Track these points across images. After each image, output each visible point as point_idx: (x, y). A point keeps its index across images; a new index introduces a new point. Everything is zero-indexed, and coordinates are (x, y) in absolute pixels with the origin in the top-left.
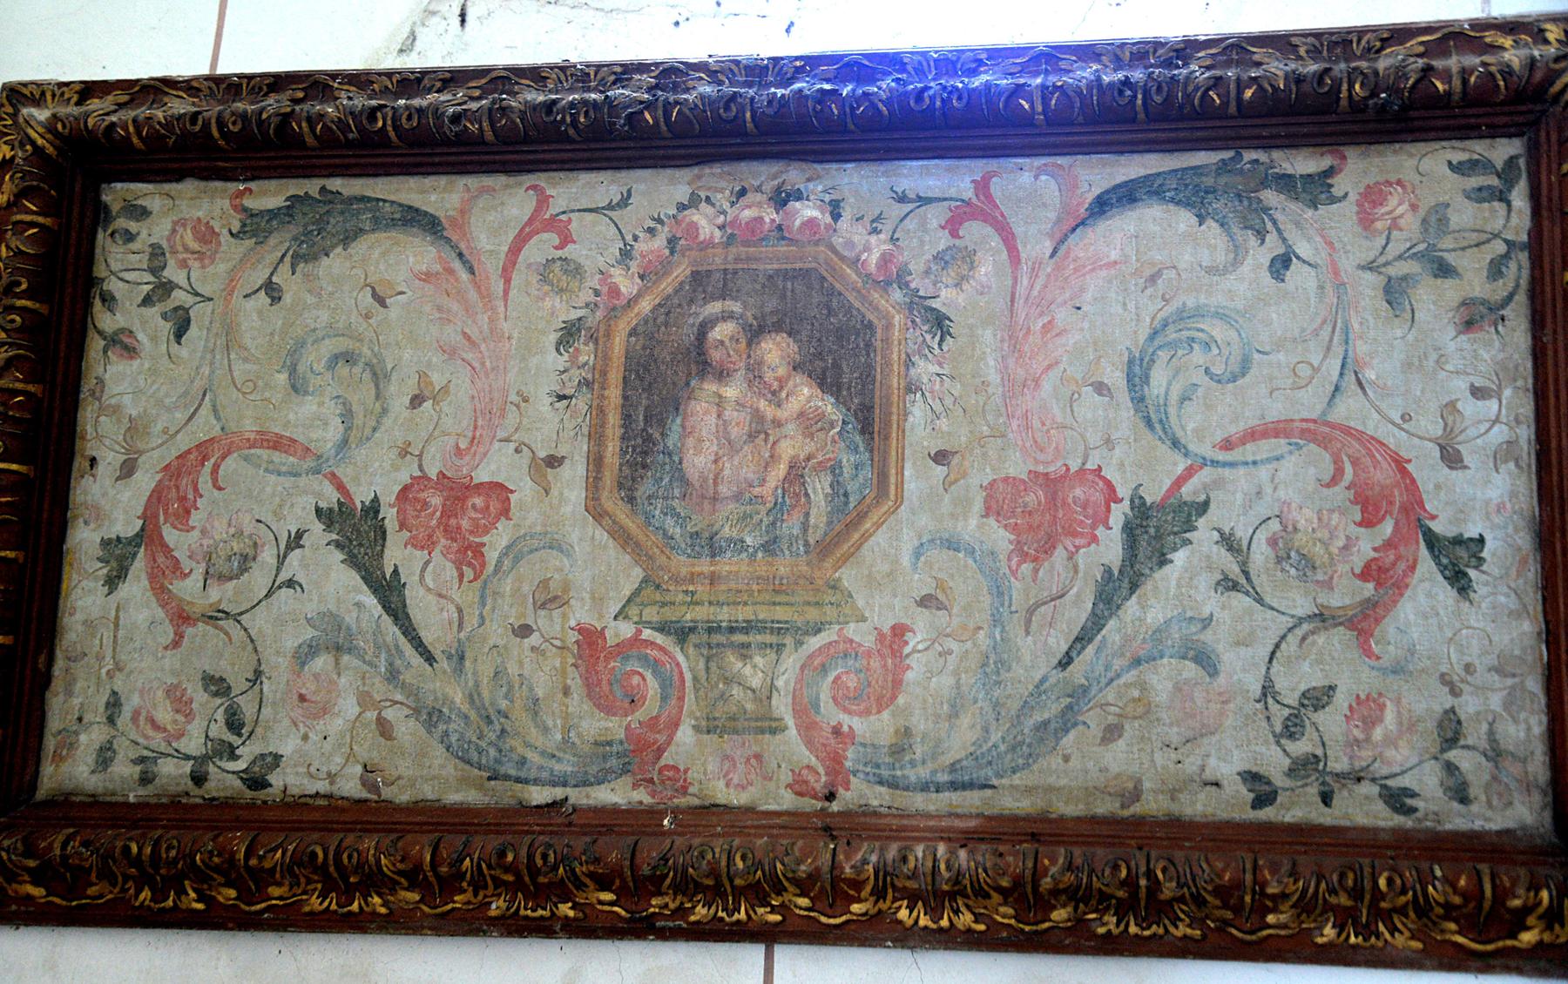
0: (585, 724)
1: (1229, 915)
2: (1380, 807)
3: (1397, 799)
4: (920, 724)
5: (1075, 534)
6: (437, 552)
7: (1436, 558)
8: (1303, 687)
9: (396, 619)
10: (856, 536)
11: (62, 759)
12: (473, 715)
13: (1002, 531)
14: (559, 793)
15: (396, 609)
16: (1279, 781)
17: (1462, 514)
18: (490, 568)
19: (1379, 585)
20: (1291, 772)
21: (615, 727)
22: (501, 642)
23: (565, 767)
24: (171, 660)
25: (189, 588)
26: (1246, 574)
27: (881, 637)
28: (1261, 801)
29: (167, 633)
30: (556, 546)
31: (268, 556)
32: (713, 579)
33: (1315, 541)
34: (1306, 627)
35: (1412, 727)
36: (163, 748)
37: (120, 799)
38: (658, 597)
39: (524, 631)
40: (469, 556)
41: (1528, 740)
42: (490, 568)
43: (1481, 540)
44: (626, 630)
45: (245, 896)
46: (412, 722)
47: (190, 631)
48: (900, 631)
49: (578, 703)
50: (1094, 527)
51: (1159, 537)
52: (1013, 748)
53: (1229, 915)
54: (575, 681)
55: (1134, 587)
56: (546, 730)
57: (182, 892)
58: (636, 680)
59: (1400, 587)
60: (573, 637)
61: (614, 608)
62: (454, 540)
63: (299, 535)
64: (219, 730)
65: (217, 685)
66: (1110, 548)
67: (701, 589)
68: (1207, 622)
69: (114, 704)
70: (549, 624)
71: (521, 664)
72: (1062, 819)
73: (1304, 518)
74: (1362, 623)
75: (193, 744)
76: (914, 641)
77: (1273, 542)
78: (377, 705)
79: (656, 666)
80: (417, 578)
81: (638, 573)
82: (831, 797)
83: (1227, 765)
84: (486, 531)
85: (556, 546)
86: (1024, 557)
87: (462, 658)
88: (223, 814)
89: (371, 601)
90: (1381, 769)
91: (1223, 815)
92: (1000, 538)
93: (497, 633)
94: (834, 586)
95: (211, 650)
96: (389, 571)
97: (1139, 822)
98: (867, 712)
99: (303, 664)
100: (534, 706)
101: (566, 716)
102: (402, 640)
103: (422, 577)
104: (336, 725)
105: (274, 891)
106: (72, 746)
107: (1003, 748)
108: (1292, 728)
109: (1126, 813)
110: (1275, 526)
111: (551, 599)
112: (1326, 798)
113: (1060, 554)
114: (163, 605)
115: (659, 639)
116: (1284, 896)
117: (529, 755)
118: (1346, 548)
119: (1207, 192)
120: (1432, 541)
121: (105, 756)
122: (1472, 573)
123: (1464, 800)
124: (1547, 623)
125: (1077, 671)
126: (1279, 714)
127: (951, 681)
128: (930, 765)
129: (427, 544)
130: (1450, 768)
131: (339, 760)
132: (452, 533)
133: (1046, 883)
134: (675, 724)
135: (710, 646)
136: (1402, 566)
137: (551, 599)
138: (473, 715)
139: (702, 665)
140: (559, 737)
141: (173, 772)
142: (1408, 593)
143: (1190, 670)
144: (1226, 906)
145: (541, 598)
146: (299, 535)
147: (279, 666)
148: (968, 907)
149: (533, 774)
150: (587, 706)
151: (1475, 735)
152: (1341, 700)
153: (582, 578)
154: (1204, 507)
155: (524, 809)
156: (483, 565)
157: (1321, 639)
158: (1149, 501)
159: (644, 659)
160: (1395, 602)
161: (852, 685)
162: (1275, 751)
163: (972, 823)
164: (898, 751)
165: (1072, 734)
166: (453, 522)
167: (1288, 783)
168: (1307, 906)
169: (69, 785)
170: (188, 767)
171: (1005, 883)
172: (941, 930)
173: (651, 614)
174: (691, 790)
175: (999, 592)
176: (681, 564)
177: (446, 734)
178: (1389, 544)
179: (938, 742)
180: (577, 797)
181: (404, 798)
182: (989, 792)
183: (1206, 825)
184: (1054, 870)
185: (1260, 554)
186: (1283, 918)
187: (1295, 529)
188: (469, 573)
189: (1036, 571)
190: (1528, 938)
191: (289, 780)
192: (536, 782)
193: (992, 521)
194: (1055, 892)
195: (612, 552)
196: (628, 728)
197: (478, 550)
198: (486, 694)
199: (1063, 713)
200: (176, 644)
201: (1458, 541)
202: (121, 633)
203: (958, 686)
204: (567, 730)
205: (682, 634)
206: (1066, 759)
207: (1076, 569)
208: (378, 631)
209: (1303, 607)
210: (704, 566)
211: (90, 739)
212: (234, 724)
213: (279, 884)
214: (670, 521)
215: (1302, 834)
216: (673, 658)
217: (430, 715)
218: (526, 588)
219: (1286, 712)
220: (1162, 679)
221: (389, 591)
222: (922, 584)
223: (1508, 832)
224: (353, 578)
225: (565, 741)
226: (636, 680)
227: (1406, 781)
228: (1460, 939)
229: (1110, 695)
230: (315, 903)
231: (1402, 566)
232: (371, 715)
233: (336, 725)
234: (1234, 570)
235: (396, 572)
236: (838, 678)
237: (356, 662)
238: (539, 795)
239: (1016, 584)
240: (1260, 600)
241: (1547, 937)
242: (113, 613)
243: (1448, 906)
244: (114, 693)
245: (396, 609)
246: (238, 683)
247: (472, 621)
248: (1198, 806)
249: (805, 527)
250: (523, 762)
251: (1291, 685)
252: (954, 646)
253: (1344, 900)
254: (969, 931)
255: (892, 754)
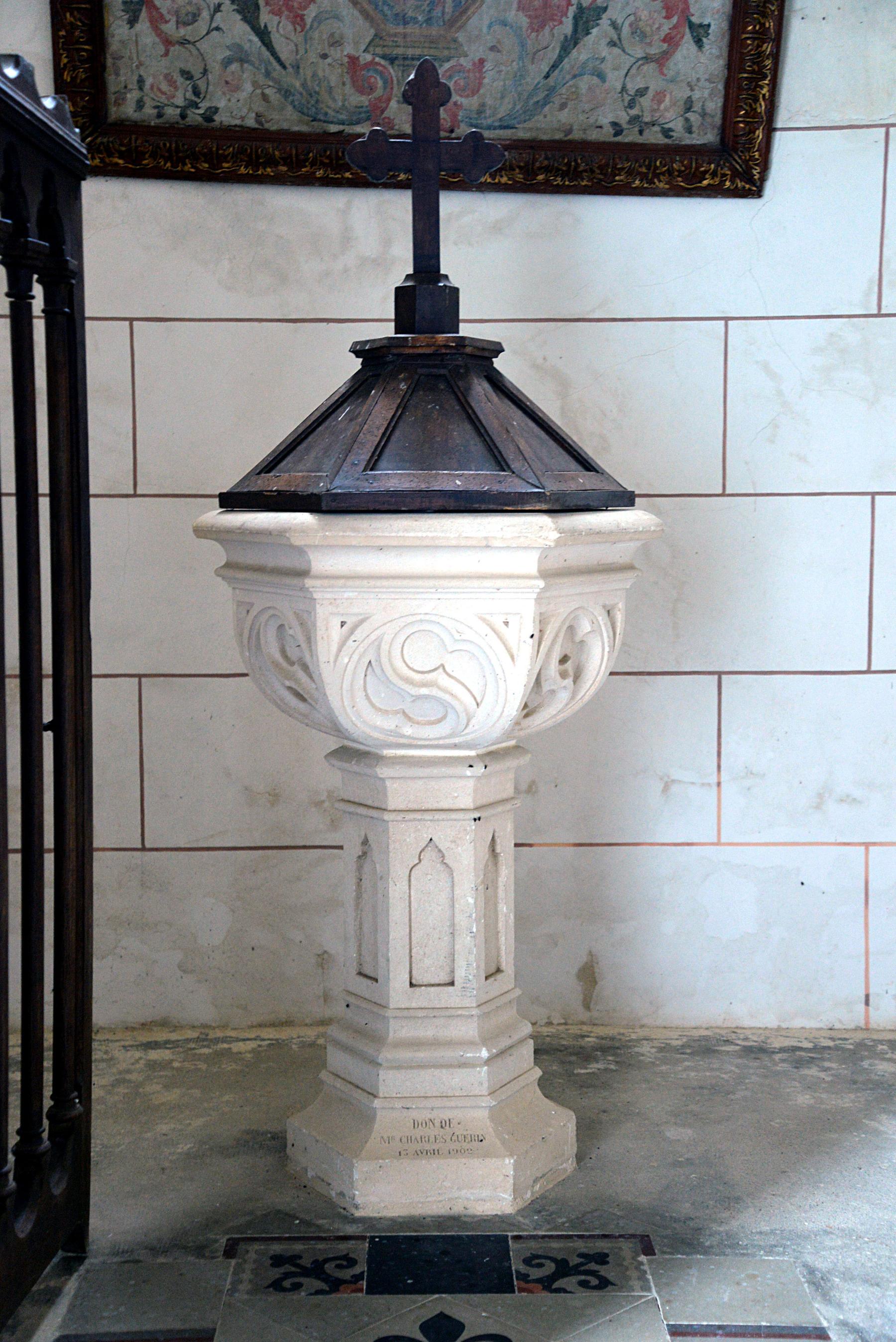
0: (351, 99)
1: (602, 177)
2: (660, 136)
3: (667, 133)
4: (489, 101)
5: (554, 20)
6: (283, 18)
7: (692, 33)
8: (637, 87)
9: (268, 49)
10: (464, 18)
11: (119, 105)
12: (304, 93)
13: (524, 18)
14: (341, 127)
15: (267, 44)
16: (625, 126)
17: (703, 14)
18: (308, 27)
19: (669, 45)
20: (629, 122)
21: (364, 100)
22: (314, 60)
23: (343, 117)
24: (164, 62)
25: (169, 28)
26: (620, 39)
27: (474, 64)
28: (616, 135)
29: (161, 49)
30: (337, 17)
31: (205, 14)
32: (405, 36)
33: (647, 25)
34: (640, 62)
35: (674, 104)
36: (166, 102)
37: (146, 124)
38: (381, 42)
39: (324, 56)
40: (298, 20)
41: (716, 109)
42: (308, 27)
43: (709, 25)
44: (368, 57)
45: (213, 166)
46: (278, 95)
47: (172, 48)
48: (482, 61)
49: (348, 89)
50: (562, 16)
51: (587, 22)
52: (525, 112)
53: (602, 177)
54: (347, 79)
55: (576, 44)
56: (334, 100)
57: (184, 164)
58: (373, 80)
59: (677, 45)
60: (346, 60)
61: (363, 47)
62: (290, 12)
63: (220, 5)
64: (190, 95)
65: (187, 75)
66: (567, 27)
67: (400, 40)
68: (603, 60)
69: (141, 81)
70: (335, 53)
71: (324, 71)
72: (541, 141)
73: (644, 15)
74: (661, 60)
75: (180, 101)
76: (488, 66)
77: (631, 25)
78: (260, 87)
79: (381, 74)
80: (275, 29)
81: (372, 31)
82: (452, 131)
83: (605, 120)
84: (305, 8)
85: (337, 17)
86: (533, 30)
87: (298, 67)
88: (195, 132)
89: (255, 39)
90: (662, 121)
91: (602, 139)
92: (524, 21)
93: (313, 57)
94: (455, 40)
95: (182, 58)
96: (262, 25)
97: (570, 142)
98: (467, 96)
99: (226, 67)
100: (330, 90)
101: (344, 95)
102: (272, 59)
103: (278, 29)
104: (243, 95)
105: (225, 165)
106: (124, 99)
107: (521, 112)
108: (631, 105)
109: (566, 139)
110: (632, 18)
111: (336, 42)
112: (641, 132)
113: (547, 29)
114: (158, 35)
115: (383, 62)
116: (623, 169)
117: (330, 111)
118: (659, 28)
119: (842, 1249)
120: (691, 26)
121: (140, 104)
122: (704, 40)
123: (690, 132)
124: (729, 60)
125: (551, 81)
126: (627, 98)
127: (502, 83)
128: (492, 119)
129: (278, 13)
130: (687, 120)
131: (246, 111)
132: (290, 9)
133: (537, 164)
134: (389, 100)
135: (404, 66)
136: (679, 36)
137: (336, 42)
138: (304, 93)
139: (400, 74)
140: (340, 104)
141: (171, 113)
142: (680, 48)
143: (595, 80)
144: (601, 174)
145: (331, 41)
146: (220, 5)
147: (215, 68)
148: (507, 175)
149: (331, 119)
150: (352, 91)
151: (697, 107)
152: (651, 93)
153: (349, 33)
154: (605, 9)
155: (327, 134)
156: (305, 24)
157: (645, 68)
158: (584, 5)
159: (376, 71)
160: (674, 52)
161: (462, 84)
162: (624, 113)
163: (508, 142)
164: (479, 112)
165: (547, 107)
166: (290, 3)
167: (628, 126)
168: (630, 172)
169: (123, 116)
170: (178, 111)
171: (522, 164)
172: (495, 184)
173: (379, 50)
174: (397, 127)
175: (523, 45)
176: (392, 28)
177: (293, 101)
178: (675, 27)
179: (495, 109)
180: (349, 129)
181: (274, 128)
182: (514, 130)
183: (595, 143)
184: (541, 160)
185: (626, 31)
186: (622, 177)
187: (640, 20)
188: (299, 29)
189: (537, 36)
190: (705, 182)
191: (222, 119)
192: (332, 122)
193: (520, 13)
194: (540, 168)
195: (361, 22)
196: (370, 101)
197: (302, 17)
198: (309, 83)
199: (544, 98)
200: (166, 54)
201: (701, 25)
202: (140, 48)
203: (504, 85)
204: (344, 100)
205: (392, 60)
206: (545, 116)
207: (553, 36)
208: (260, 54)
209: (640, 54)
210: (400, 29)
211: (132, 96)
212: (196, 92)
213: (228, 162)
214: (386, 8)
215: (632, 146)
216: (388, 71)
217: (286, 92)
218: (325, 37)
219: (630, 98)
220: (584, 83)
221: (263, 35)
222: (490, 40)
223: (705, 144)
224: (247, 28)
225: (343, 105)
226: (373, 80)
227: (670, 125)
228: (682, 184)
229: (564, 91)
230: (243, 170)
231: (679, 36)
232: (259, 91)
233: (243, 95)
234: (615, 38)
235: (266, 26)
236: (456, 82)
237: (250, 67)
238: (333, 128)
239: (529, 42)
240: (624, 51)
241: (712, 182)
242: (134, 38)
243: (679, 171)
244: (140, 76)
245: (267, 44)
246: (197, 75)
247: (302, 52)
248: (594, 136)
249: (443, 13)
250: (326, 114)
251: (632, 88)
252: (504, 68)
253: (644, 170)
254: (506, 184)
255: (477, 114)
